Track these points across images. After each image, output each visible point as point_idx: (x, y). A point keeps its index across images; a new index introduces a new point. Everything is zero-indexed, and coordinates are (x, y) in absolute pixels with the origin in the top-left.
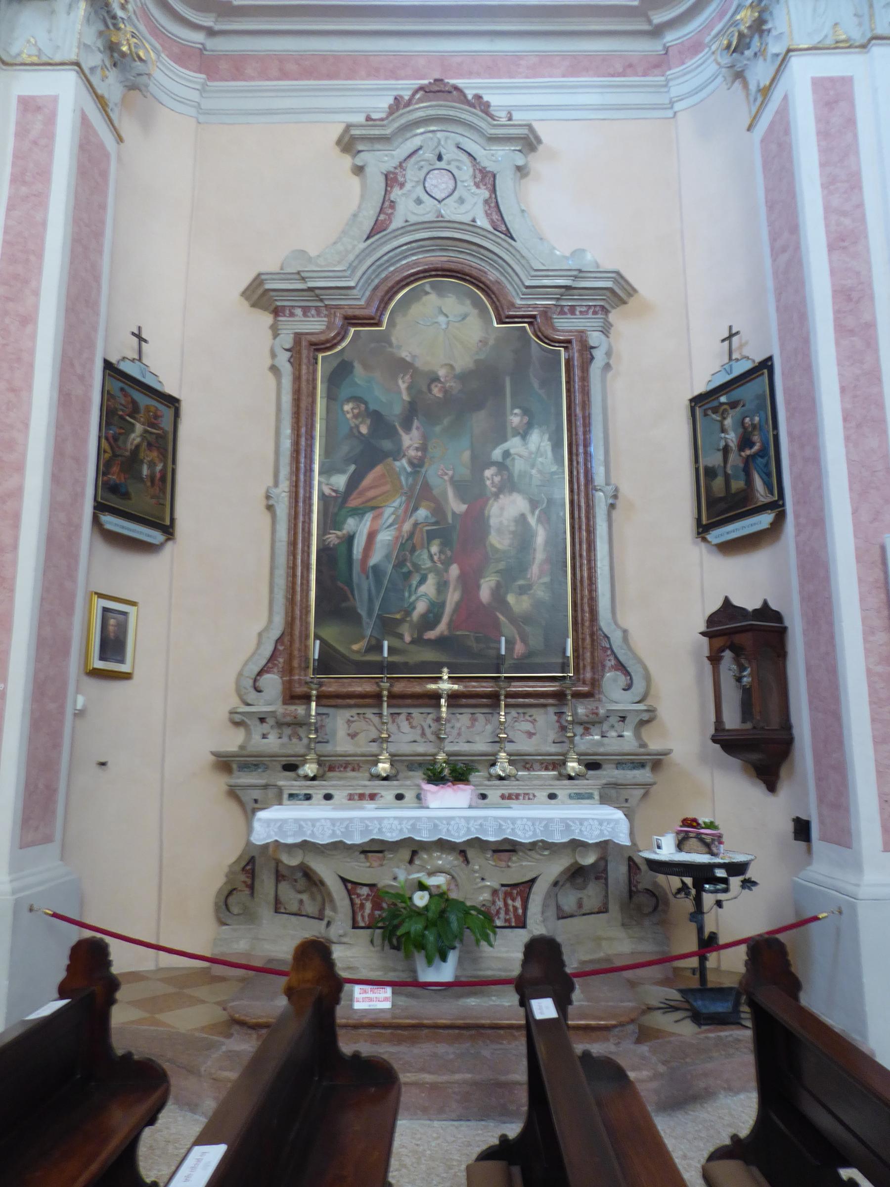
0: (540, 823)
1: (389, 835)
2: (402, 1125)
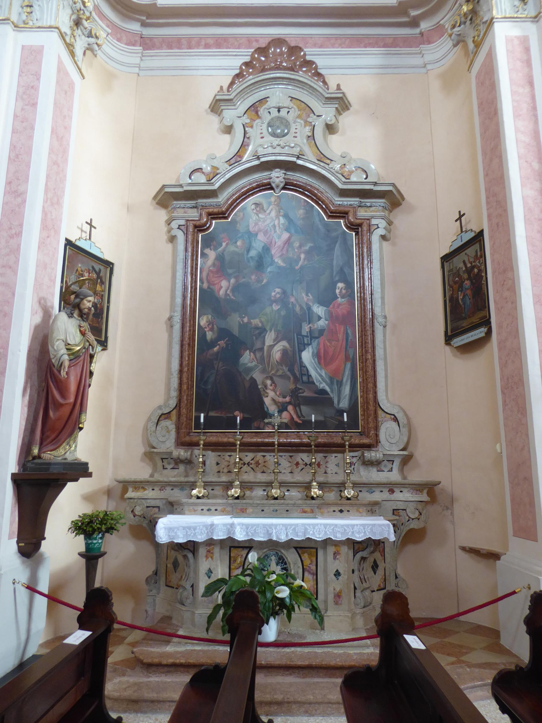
0: (368, 527)
1: (199, 537)
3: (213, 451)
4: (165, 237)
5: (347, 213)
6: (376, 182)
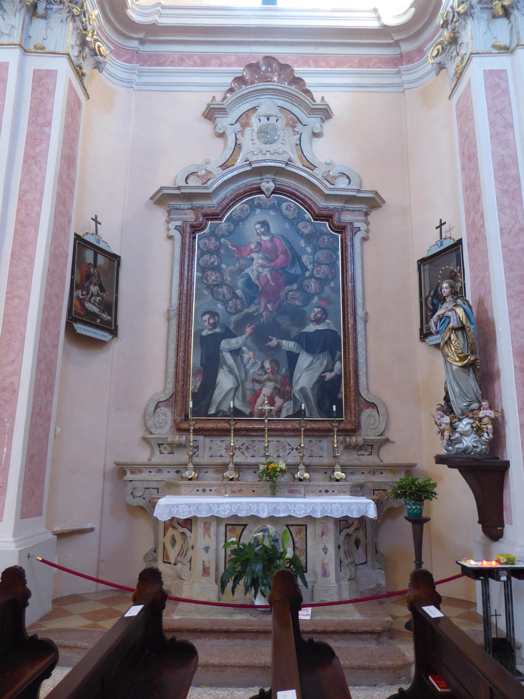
0: (310, 506)
2: (191, 687)
3: (205, 436)
4: (164, 235)
5: (331, 217)
6: (358, 190)
